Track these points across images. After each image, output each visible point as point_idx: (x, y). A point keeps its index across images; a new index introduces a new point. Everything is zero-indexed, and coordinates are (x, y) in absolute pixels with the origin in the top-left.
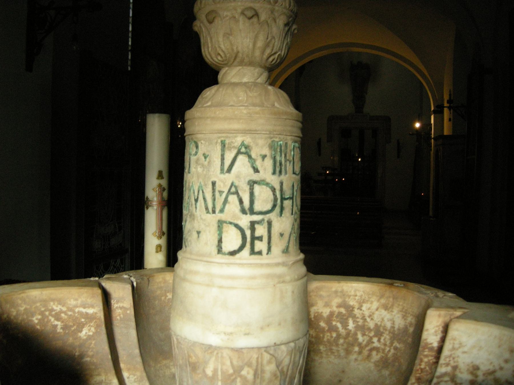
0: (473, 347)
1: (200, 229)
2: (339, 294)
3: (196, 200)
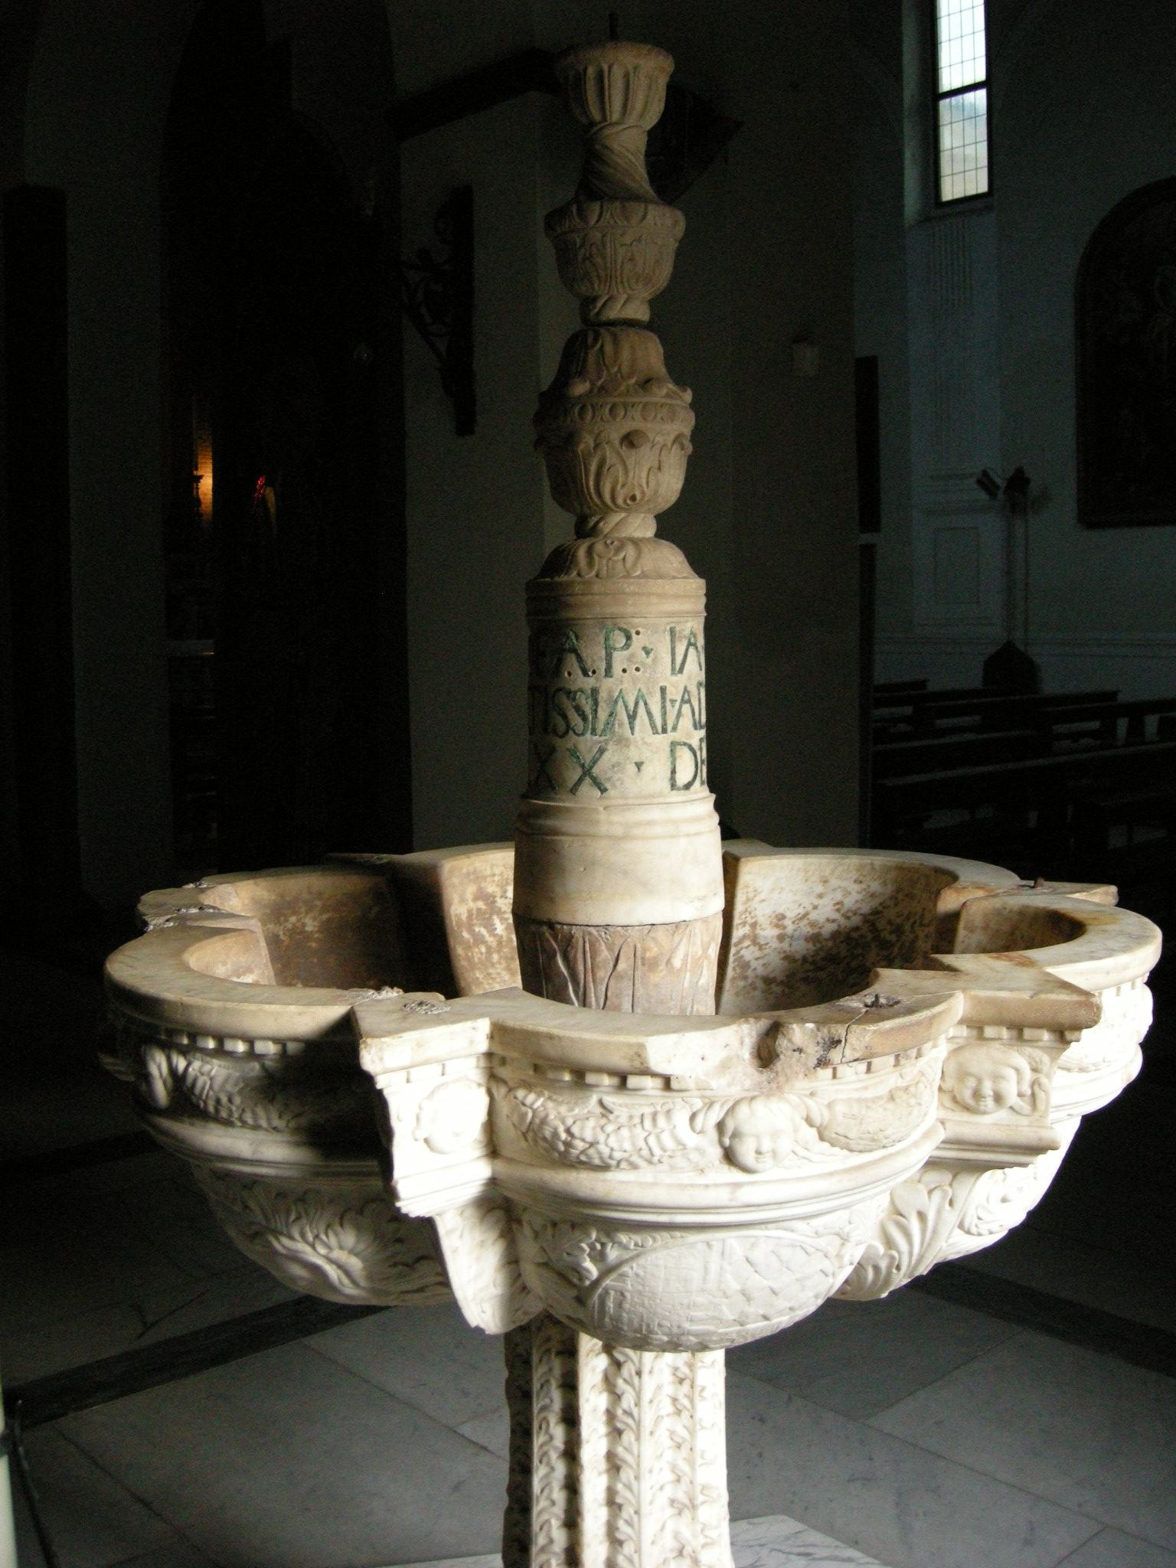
0: (773, 890)
1: (643, 759)
3: (632, 717)
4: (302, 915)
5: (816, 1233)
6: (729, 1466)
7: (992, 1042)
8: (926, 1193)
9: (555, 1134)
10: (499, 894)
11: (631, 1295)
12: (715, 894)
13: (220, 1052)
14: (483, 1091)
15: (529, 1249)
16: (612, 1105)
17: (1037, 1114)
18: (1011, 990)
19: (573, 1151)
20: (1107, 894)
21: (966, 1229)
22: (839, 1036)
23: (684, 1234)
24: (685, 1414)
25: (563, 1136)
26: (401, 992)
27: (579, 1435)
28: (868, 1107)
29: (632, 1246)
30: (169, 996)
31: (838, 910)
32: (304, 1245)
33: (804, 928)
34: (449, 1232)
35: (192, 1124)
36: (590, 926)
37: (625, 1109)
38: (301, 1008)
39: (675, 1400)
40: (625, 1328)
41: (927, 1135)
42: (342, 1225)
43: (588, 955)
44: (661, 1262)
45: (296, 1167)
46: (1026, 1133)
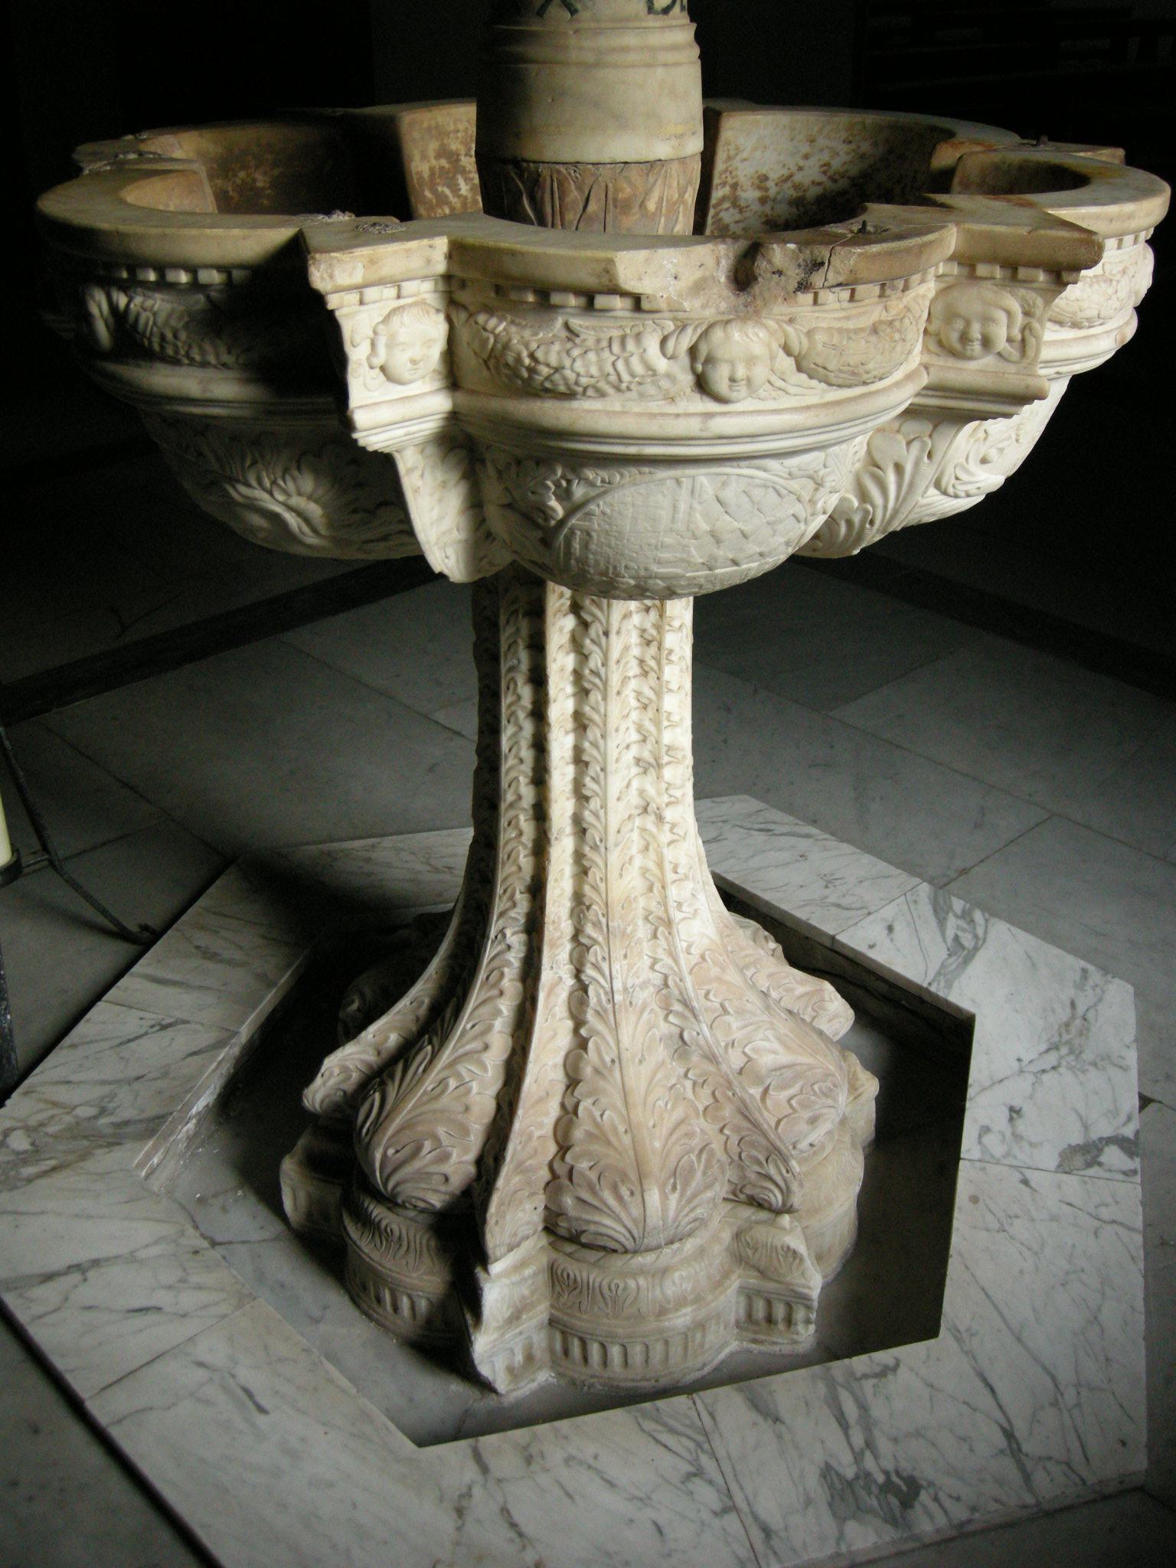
0: (755, 149)
2: (434, 131)
4: (253, 170)
5: (790, 474)
6: (693, 732)
7: (985, 282)
8: (904, 443)
9: (519, 359)
10: (463, 152)
11: (598, 535)
12: (693, 133)
13: (163, 285)
14: (441, 317)
15: (493, 491)
16: (579, 328)
17: (1025, 362)
18: (1008, 225)
19: (537, 377)
20: (1114, 156)
21: (943, 487)
22: (822, 258)
23: (652, 470)
24: (652, 675)
25: (527, 361)
26: (353, 217)
27: (546, 694)
28: (849, 338)
29: (599, 483)
30: (104, 225)
31: (825, 173)
32: (262, 492)
33: (788, 192)
34: (410, 471)
35: (138, 366)
36: (559, 163)
37: (592, 333)
38: (246, 232)
39: (641, 662)
40: (592, 571)
41: (909, 377)
42: (299, 469)
43: (556, 195)
44: (629, 499)
45: (248, 405)
46: (1012, 379)
